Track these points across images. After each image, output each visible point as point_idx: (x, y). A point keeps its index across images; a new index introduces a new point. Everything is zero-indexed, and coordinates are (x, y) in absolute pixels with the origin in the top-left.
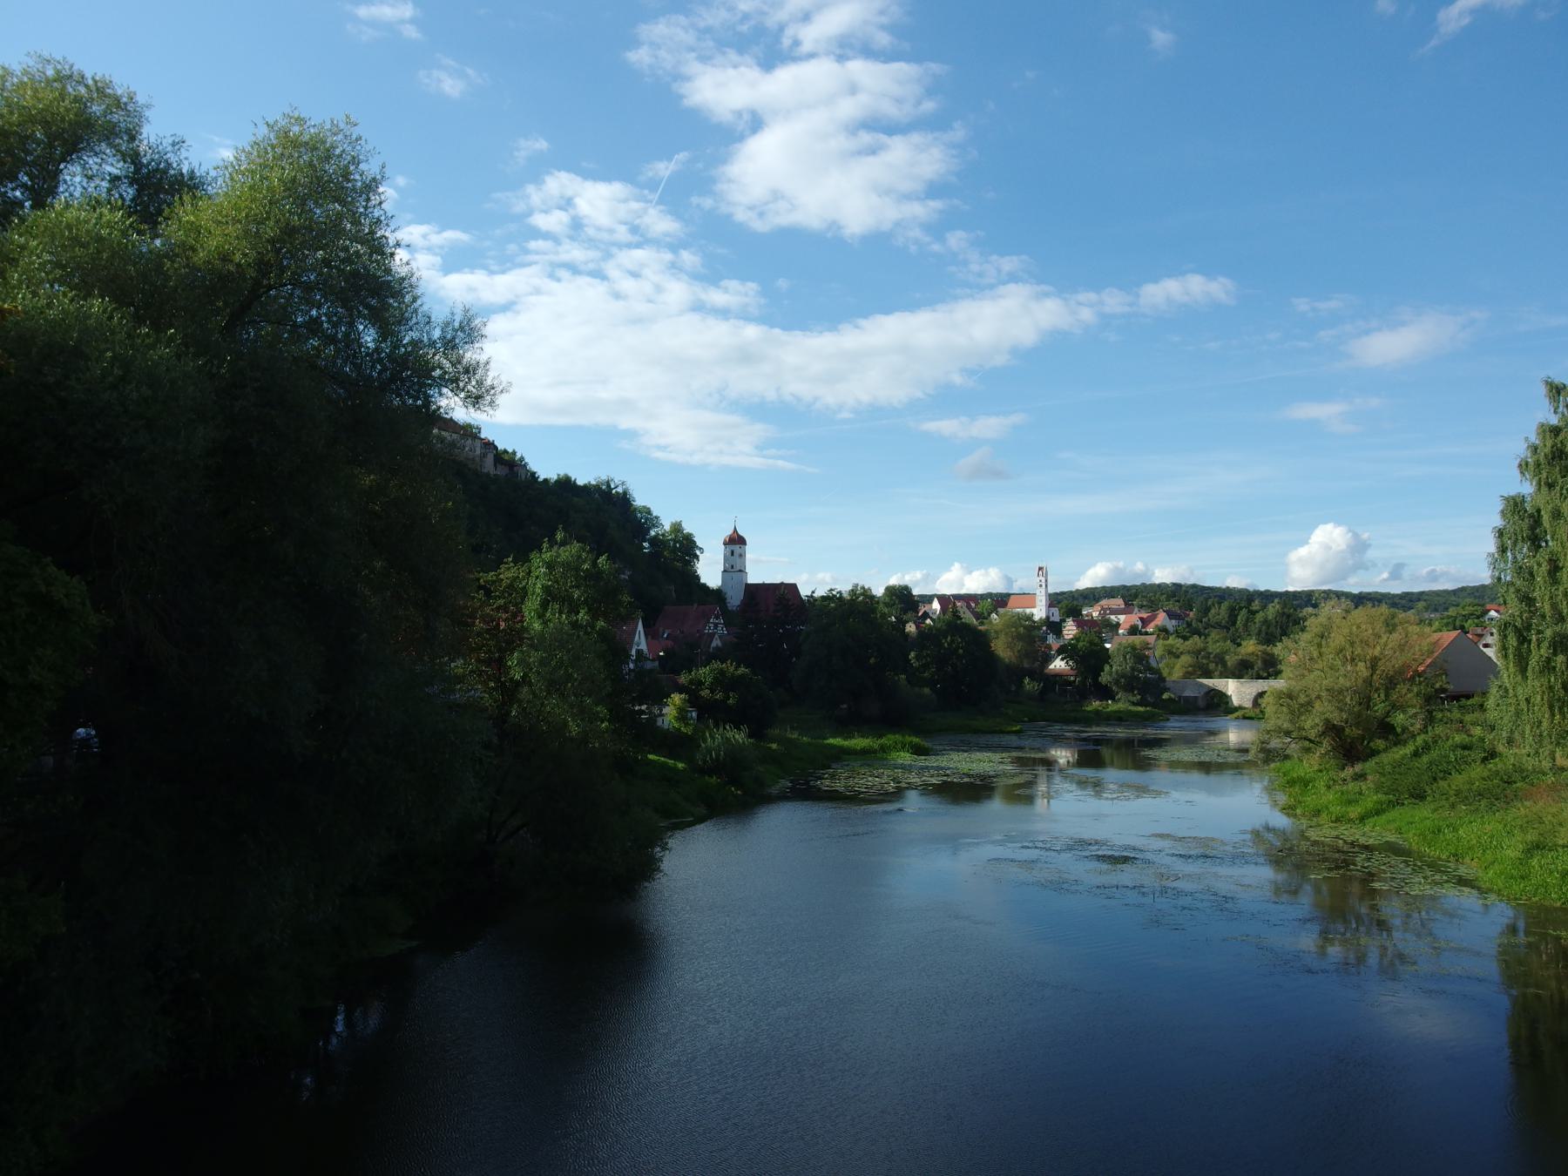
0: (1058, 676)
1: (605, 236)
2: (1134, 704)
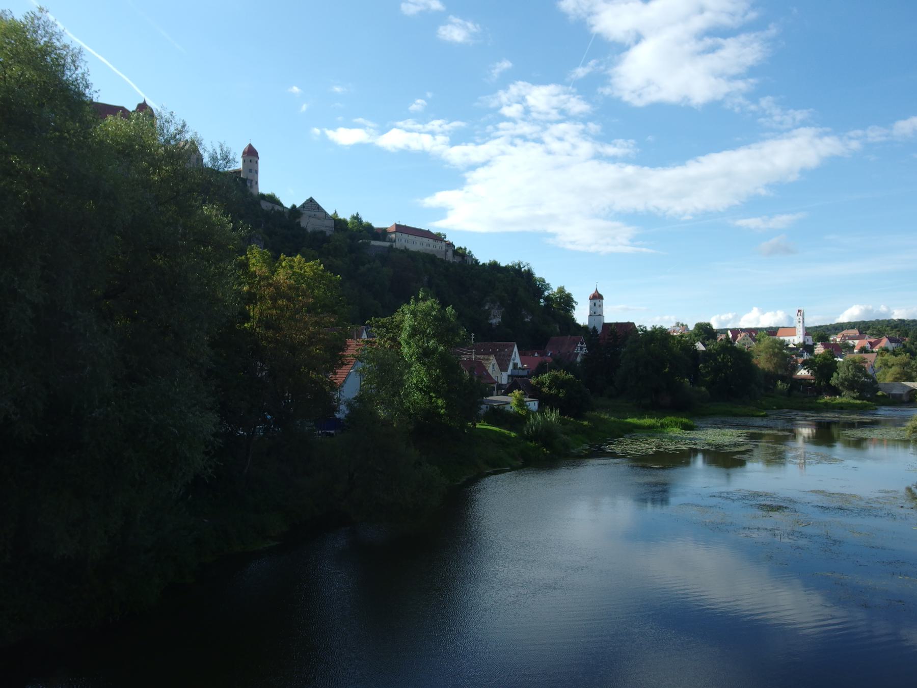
0: (803, 380)
1: (543, 117)
2: (854, 398)
